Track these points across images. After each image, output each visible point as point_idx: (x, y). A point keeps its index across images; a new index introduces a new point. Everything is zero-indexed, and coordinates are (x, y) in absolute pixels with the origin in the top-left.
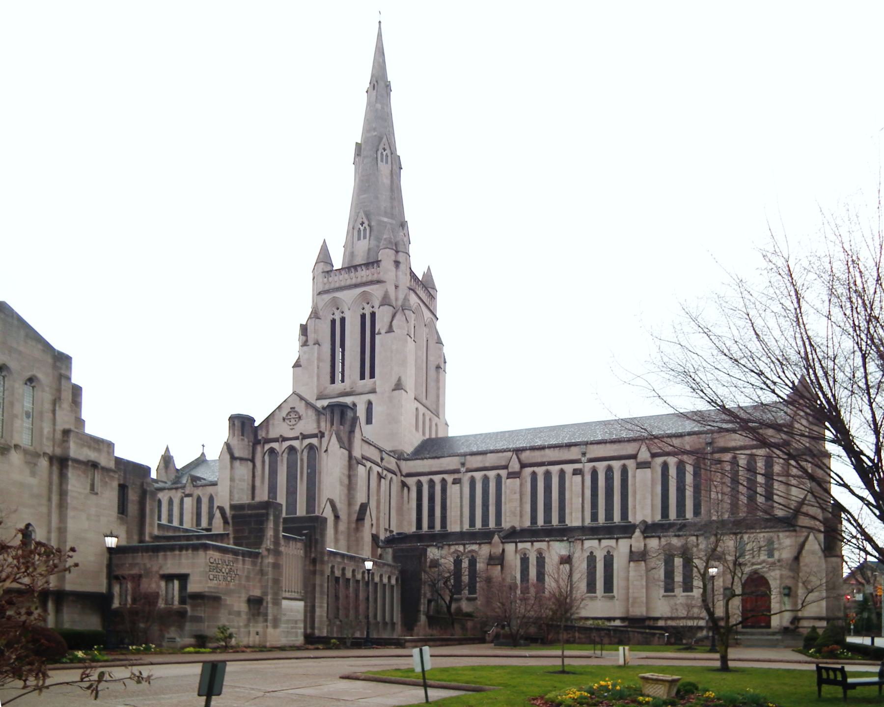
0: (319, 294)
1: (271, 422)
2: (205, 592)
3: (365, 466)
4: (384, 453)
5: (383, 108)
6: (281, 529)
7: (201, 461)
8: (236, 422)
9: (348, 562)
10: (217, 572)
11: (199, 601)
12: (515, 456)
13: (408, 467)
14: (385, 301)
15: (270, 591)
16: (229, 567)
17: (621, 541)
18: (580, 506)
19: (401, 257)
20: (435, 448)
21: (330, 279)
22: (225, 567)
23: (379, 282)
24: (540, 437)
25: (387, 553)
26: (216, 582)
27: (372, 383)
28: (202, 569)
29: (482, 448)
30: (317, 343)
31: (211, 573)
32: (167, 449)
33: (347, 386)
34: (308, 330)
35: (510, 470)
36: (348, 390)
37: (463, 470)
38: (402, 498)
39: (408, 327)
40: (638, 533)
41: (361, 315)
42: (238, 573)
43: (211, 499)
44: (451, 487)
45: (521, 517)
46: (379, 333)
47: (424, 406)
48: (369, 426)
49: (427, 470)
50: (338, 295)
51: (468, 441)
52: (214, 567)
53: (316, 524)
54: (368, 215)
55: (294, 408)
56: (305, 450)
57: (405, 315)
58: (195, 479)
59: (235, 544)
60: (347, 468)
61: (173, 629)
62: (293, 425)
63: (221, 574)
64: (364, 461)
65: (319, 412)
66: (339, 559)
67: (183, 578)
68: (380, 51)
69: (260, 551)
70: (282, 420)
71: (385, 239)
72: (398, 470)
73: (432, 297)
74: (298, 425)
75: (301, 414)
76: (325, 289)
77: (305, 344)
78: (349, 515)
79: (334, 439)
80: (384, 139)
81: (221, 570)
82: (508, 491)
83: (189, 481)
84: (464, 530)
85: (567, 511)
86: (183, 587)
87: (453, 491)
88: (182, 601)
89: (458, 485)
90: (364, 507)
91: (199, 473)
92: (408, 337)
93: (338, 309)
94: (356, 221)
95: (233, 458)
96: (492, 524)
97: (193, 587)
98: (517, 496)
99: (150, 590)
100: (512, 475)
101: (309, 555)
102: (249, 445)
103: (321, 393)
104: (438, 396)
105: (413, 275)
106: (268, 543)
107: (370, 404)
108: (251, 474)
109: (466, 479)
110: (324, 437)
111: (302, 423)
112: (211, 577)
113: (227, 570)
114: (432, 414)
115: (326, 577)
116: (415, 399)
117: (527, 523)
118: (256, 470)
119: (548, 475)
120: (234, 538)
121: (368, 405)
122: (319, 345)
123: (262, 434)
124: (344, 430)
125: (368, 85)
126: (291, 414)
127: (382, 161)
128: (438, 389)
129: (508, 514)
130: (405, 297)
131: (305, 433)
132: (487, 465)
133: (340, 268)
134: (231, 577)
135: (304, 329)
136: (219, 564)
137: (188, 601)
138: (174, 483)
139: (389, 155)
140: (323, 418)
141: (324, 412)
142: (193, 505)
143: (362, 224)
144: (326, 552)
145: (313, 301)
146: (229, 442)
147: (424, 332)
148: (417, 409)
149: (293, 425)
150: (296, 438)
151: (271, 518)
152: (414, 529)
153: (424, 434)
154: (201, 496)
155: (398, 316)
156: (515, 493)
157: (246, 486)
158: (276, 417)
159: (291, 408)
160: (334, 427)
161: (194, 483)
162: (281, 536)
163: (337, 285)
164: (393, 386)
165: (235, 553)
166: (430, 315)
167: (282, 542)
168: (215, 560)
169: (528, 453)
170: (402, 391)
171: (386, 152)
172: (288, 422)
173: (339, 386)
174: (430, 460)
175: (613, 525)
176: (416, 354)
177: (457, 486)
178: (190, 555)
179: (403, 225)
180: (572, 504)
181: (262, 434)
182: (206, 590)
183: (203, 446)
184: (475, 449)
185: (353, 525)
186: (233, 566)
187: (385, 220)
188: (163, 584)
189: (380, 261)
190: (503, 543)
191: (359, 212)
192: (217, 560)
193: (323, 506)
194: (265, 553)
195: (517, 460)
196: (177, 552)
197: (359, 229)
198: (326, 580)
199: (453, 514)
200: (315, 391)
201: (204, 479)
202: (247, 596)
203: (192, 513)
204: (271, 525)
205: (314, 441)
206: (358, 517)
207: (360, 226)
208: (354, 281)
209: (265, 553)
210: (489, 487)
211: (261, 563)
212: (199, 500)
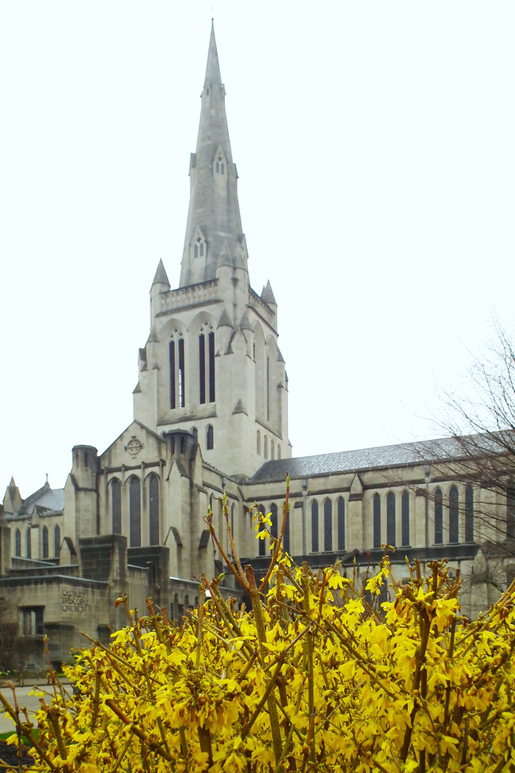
0: (157, 316)
1: (113, 452)
2: (60, 622)
3: (206, 493)
4: (225, 479)
5: (217, 114)
6: (126, 560)
7: (45, 491)
8: (80, 453)
9: (191, 590)
10: (69, 603)
11: (55, 630)
12: (357, 478)
13: (250, 491)
14: (224, 322)
15: (118, 620)
16: (80, 598)
17: (463, 563)
18: (424, 528)
19: (239, 274)
20: (277, 471)
21: (168, 300)
22: (76, 598)
23: (217, 301)
24: (383, 457)
25: (230, 579)
26: (69, 612)
27: (213, 406)
28: (56, 601)
29: (324, 469)
30: (156, 367)
31: (63, 604)
32: (12, 480)
33: (187, 410)
34: (147, 354)
35: (353, 492)
36: (188, 414)
37: (305, 493)
38: (245, 523)
39: (248, 347)
40: (479, 554)
42: (89, 603)
43: (57, 529)
44: (293, 512)
45: (364, 539)
46: (218, 355)
47: (266, 428)
48: (210, 451)
49: (269, 494)
50: (176, 316)
51: (310, 463)
52: (67, 599)
53: (159, 555)
54: (204, 230)
56: (147, 479)
57: (244, 335)
58: (40, 510)
59: (85, 576)
60: (188, 496)
61: (31, 656)
62: (135, 454)
63: (73, 605)
64: (205, 488)
65: (160, 440)
66: (182, 588)
67: (39, 610)
68: (213, 52)
69: (108, 582)
70: (123, 449)
71: (223, 256)
72: (240, 495)
73: (272, 313)
74: (140, 453)
75: (142, 443)
76: (163, 311)
77: (144, 369)
78: (192, 542)
79: (175, 467)
80: (220, 149)
81: (73, 602)
82: (350, 514)
83: (35, 512)
84: (307, 554)
85: (411, 533)
86: (40, 618)
87: (296, 515)
88: (40, 631)
89: (300, 509)
90: (205, 535)
91: (44, 503)
92: (248, 357)
93: (176, 331)
94: (192, 238)
95: (78, 489)
96: (335, 548)
97: (49, 617)
98: (360, 519)
99: (11, 622)
100: (354, 497)
101: (153, 584)
102: (92, 476)
103: (162, 418)
104: (280, 417)
105: (252, 293)
106: (115, 575)
107: (210, 428)
108: (95, 504)
109: (308, 502)
110: (165, 465)
111: (143, 452)
112: (65, 608)
113: (78, 602)
114: (274, 436)
115: (170, 605)
116: (256, 421)
117: (370, 546)
118: (100, 500)
119: (391, 496)
120: (84, 570)
121: (209, 429)
122: (158, 369)
123: (105, 464)
124: (185, 458)
125: (202, 89)
126: (133, 443)
128: (280, 409)
129: (350, 537)
130: (244, 315)
131: (147, 462)
132: (329, 487)
133: (177, 288)
134: (82, 607)
135: (143, 353)
136: (71, 596)
137: (44, 630)
138: (21, 514)
139: (225, 164)
140: (163, 446)
141: (165, 440)
142: (39, 535)
143: (199, 240)
144: (169, 581)
145: (151, 324)
146: (73, 473)
147: (263, 351)
148: (258, 432)
149: (135, 454)
150: (138, 467)
151: (117, 551)
152: (257, 554)
153: (266, 456)
154: (47, 526)
155: (237, 337)
156: (357, 516)
157: (91, 516)
158: (118, 447)
159: (135, 458)
160: (175, 455)
161: (41, 514)
162: (126, 568)
163: (175, 306)
164: (233, 409)
165: (85, 585)
166: (270, 332)
167: (128, 573)
168: (67, 592)
169: (370, 474)
170: (243, 414)
172: (129, 451)
173: (179, 411)
174: (271, 484)
175: (457, 546)
176: (256, 372)
177: (299, 510)
178: (45, 589)
179: (241, 238)
180: (415, 525)
181: (105, 464)
182: (61, 620)
183: (47, 475)
184: (317, 472)
185: (196, 553)
186: (83, 597)
187: (222, 234)
188: (21, 615)
189: (218, 279)
190: (344, 567)
191: (195, 228)
192: (69, 592)
193: (166, 534)
194: (112, 584)
195: (359, 482)
196: (33, 586)
197: (196, 245)
198: (170, 608)
199: (295, 538)
200: (156, 417)
201: (50, 509)
202: (97, 625)
203: (39, 544)
204: (117, 558)
205: (156, 470)
206: (200, 544)
207: (197, 243)
208: (191, 302)
209: (112, 584)
210: (331, 509)
211: (109, 593)
212: (45, 531)
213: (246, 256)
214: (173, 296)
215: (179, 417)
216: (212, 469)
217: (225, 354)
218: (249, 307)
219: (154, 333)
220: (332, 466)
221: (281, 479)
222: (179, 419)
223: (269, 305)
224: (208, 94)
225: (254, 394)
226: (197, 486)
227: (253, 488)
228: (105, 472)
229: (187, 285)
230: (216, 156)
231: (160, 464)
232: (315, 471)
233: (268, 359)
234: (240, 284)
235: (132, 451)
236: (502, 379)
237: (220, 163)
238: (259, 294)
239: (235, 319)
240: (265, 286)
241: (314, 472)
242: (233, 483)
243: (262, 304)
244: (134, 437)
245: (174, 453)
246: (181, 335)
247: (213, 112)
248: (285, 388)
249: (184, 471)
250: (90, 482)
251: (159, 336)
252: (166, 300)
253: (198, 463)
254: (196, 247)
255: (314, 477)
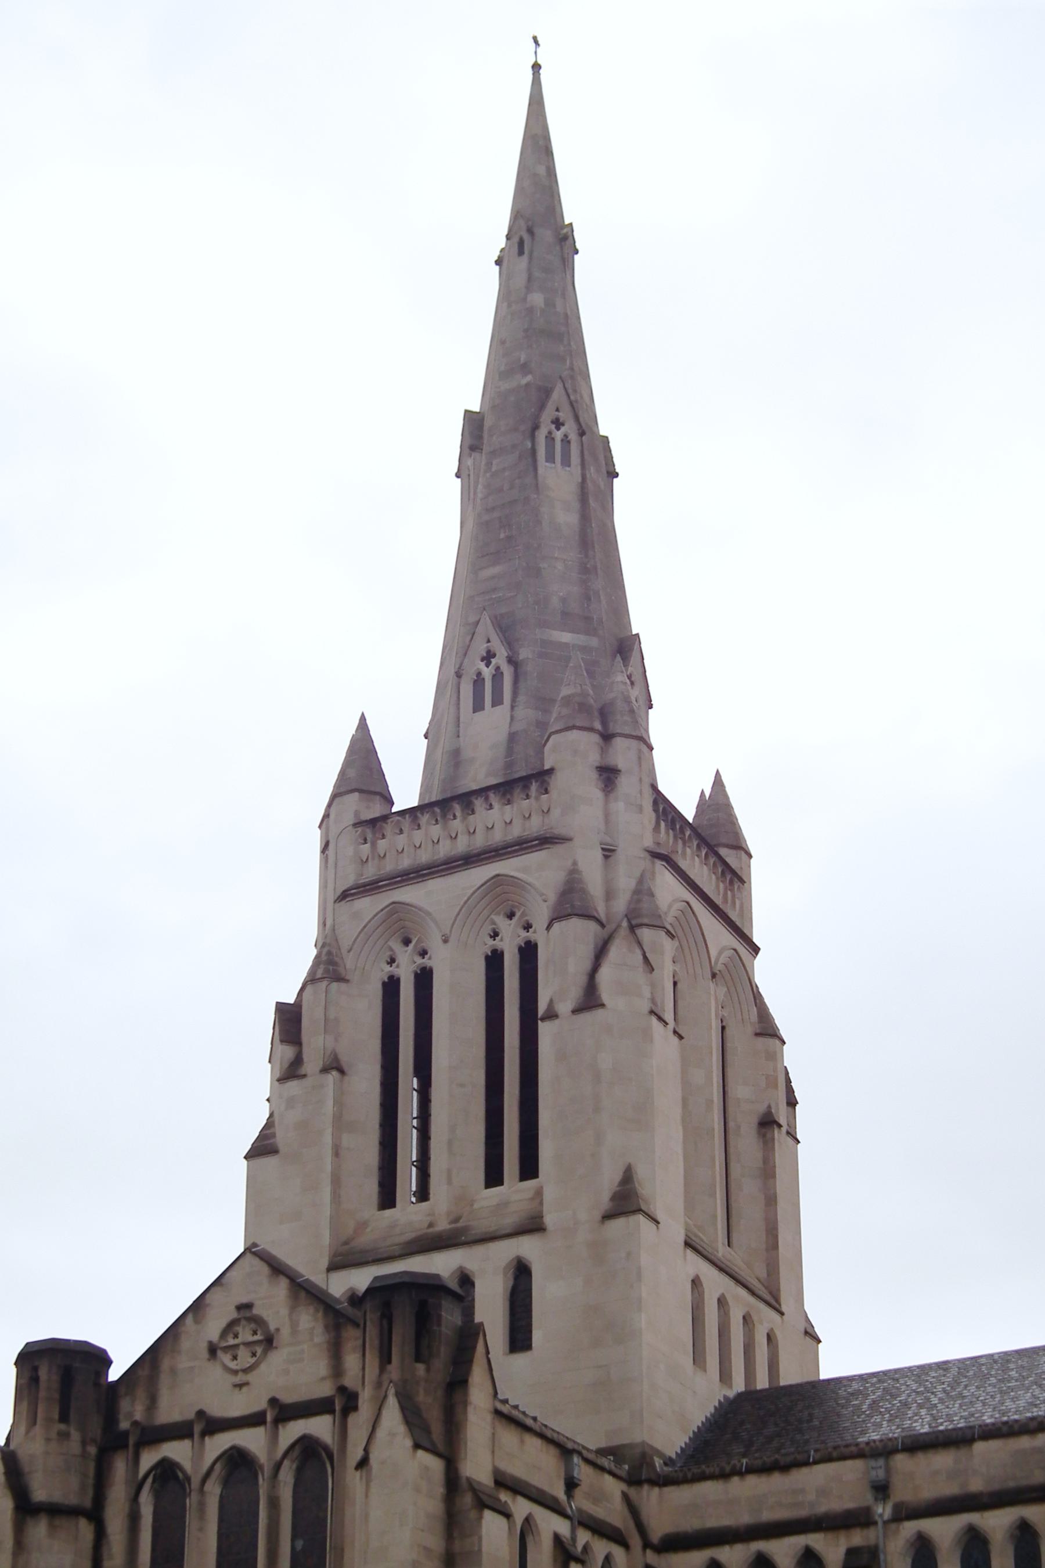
1: (166, 1364)
3: (508, 1516)
4: (576, 1459)
5: (549, 304)
19: (622, 754)
23: (546, 841)
27: (530, 1194)
29: (949, 1418)
30: (335, 1066)
36: (443, 1225)
37: (883, 1511)
41: (487, 958)
46: (551, 1015)
47: (721, 1269)
48: (521, 1359)
50: (407, 894)
51: (894, 1396)
54: (506, 629)
55: (248, 1306)
56: (286, 1463)
57: (640, 944)
62: (246, 1371)
64: (504, 1496)
70: (205, 1354)
71: (567, 701)
72: (631, 1525)
74: (263, 1367)
75: (272, 1327)
79: (392, 1416)
80: (557, 395)
92: (654, 1020)
93: (407, 942)
102: (84, 1455)
103: (346, 1243)
107: (522, 1272)
110: (355, 1408)
111: (276, 1359)
114: (752, 1300)
116: (688, 1244)
122: (342, 1071)
125: (502, 243)
126: (239, 1329)
127: (550, 458)
128: (771, 1200)
130: (641, 881)
132: (976, 1485)
139: (573, 437)
143: (488, 657)
148: (696, 1283)
149: (246, 1371)
150: (255, 1420)
153: (725, 1376)
155: (616, 952)
159: (247, 1384)
160: (394, 1370)
163: (406, 862)
164: (604, 1200)
166: (728, 939)
170: (641, 1218)
171: (563, 429)
172: (226, 1358)
174: (752, 1480)
176: (684, 1072)
184: (922, 1427)
189: (551, 771)
197: (479, 674)
200: (326, 1239)
205: (320, 1427)
207: (482, 666)
208: (462, 845)
213: (642, 701)
214: (401, 832)
215: (409, 1236)
216: (529, 1422)
217: (576, 1011)
218: (656, 855)
219: (329, 953)
220: (979, 1406)
221: (789, 1459)
222: (409, 1243)
223: (723, 852)
224: (521, 252)
225: (679, 1149)
226: (473, 1488)
227: (680, 1495)
228: (132, 1441)
229: (449, 795)
230: (547, 417)
231: (338, 1407)
232: (917, 1426)
233: (723, 1028)
234: (626, 784)
235: (235, 1358)
236: (1000, 1402)
237: (558, 435)
238: (689, 814)
239: (609, 895)
240: (707, 794)
241: (910, 1428)
242: (608, 1478)
243: (699, 847)
244: (244, 1307)
245: (390, 1362)
246: (423, 953)
247: (537, 299)
248: (784, 1129)
249: (428, 1431)
250: (74, 1482)
251: (349, 962)
252: (374, 845)
253: (478, 1396)
254: (478, 681)
255: (916, 1445)
